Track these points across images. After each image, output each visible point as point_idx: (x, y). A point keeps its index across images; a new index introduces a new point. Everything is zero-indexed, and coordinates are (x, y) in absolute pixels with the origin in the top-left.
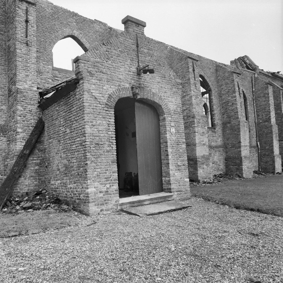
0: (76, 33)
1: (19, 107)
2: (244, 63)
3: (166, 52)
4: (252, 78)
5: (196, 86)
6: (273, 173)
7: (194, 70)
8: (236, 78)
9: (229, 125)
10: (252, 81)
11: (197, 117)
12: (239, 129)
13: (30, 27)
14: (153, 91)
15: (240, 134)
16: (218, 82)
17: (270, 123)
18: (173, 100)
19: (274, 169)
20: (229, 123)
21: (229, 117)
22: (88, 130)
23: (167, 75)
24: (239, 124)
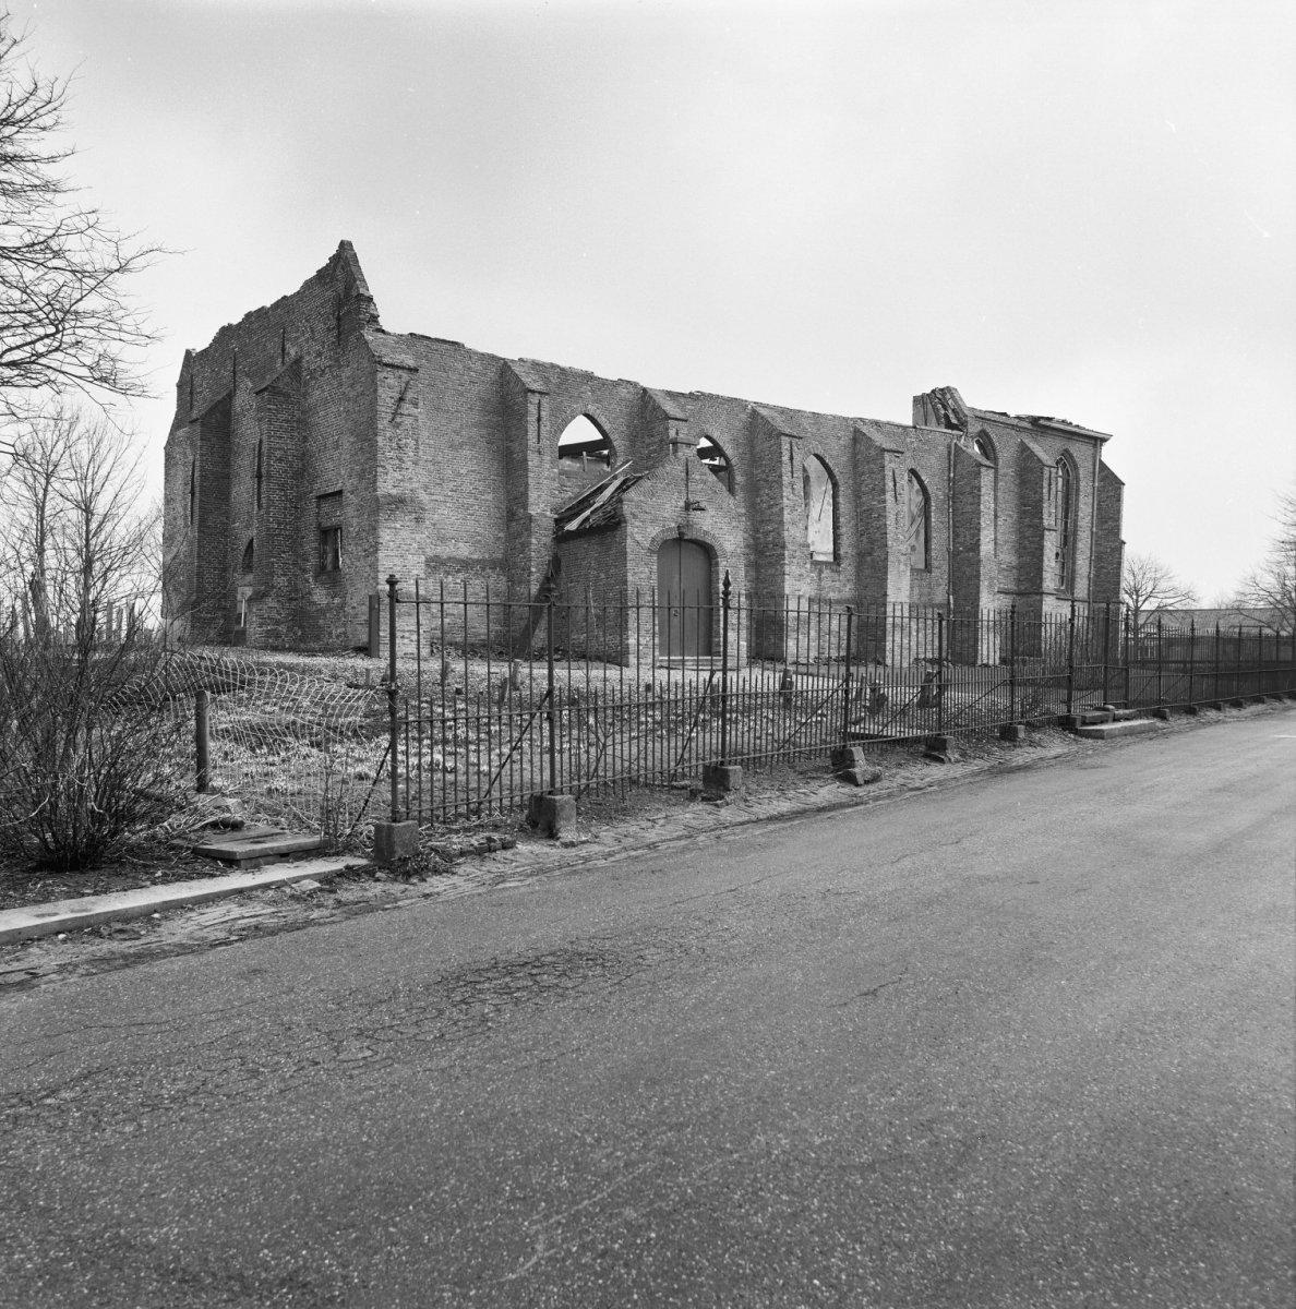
0: (591, 409)
1: (534, 541)
2: (938, 406)
3: (743, 416)
4: (949, 447)
5: (793, 489)
6: (974, 664)
7: (791, 458)
8: (891, 462)
9: (869, 559)
10: (949, 452)
11: (789, 546)
12: (886, 567)
13: (542, 427)
14: (705, 528)
15: (886, 579)
16: (855, 466)
17: (979, 554)
18: (731, 538)
19: (976, 656)
20: (870, 554)
21: (872, 542)
22: (630, 578)
23: (725, 505)
24: (886, 559)
